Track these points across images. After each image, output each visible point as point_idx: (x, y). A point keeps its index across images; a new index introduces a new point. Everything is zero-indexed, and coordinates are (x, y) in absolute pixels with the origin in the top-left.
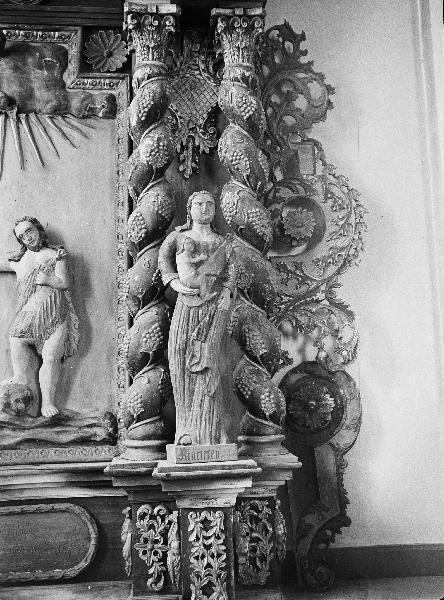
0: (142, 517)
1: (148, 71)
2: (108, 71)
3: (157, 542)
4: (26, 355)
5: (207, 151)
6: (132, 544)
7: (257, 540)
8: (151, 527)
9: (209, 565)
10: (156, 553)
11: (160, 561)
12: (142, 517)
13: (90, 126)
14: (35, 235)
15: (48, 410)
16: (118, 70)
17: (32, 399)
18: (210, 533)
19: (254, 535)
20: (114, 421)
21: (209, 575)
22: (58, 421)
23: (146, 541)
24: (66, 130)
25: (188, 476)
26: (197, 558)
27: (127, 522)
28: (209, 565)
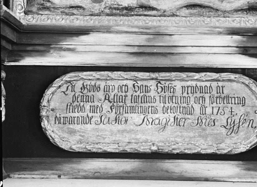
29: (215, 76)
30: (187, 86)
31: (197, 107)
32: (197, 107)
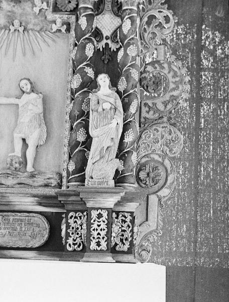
0: (71, 218)
1: (19, 8)
2: (66, 11)
3: (78, 228)
4: (21, 142)
5: (115, 50)
6: (67, 230)
7: (124, 231)
8: (75, 222)
9: (99, 234)
10: (78, 234)
11: (79, 237)
12: (71, 218)
13: (54, 41)
14: (29, 86)
15: (30, 168)
16: (71, 11)
17: (24, 162)
18: (101, 220)
19: (123, 228)
20: (61, 177)
21: (98, 222)
22: (32, 176)
23: (73, 228)
24: (46, 39)
25: (82, 63)
26: (104, 230)
27: (64, 220)
28: (99, 226)
29: (27, 214)
30: (18, 105)
31: (19, 228)
32: (19, 228)
